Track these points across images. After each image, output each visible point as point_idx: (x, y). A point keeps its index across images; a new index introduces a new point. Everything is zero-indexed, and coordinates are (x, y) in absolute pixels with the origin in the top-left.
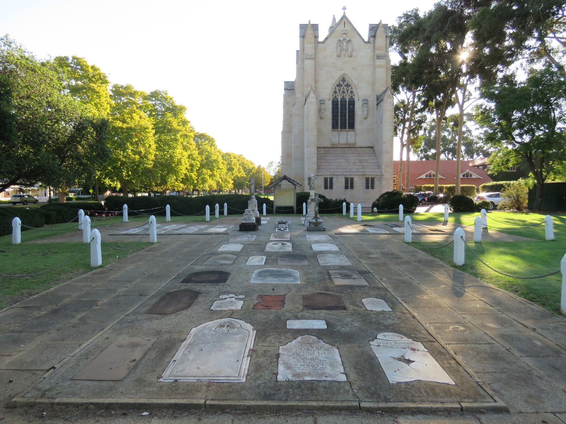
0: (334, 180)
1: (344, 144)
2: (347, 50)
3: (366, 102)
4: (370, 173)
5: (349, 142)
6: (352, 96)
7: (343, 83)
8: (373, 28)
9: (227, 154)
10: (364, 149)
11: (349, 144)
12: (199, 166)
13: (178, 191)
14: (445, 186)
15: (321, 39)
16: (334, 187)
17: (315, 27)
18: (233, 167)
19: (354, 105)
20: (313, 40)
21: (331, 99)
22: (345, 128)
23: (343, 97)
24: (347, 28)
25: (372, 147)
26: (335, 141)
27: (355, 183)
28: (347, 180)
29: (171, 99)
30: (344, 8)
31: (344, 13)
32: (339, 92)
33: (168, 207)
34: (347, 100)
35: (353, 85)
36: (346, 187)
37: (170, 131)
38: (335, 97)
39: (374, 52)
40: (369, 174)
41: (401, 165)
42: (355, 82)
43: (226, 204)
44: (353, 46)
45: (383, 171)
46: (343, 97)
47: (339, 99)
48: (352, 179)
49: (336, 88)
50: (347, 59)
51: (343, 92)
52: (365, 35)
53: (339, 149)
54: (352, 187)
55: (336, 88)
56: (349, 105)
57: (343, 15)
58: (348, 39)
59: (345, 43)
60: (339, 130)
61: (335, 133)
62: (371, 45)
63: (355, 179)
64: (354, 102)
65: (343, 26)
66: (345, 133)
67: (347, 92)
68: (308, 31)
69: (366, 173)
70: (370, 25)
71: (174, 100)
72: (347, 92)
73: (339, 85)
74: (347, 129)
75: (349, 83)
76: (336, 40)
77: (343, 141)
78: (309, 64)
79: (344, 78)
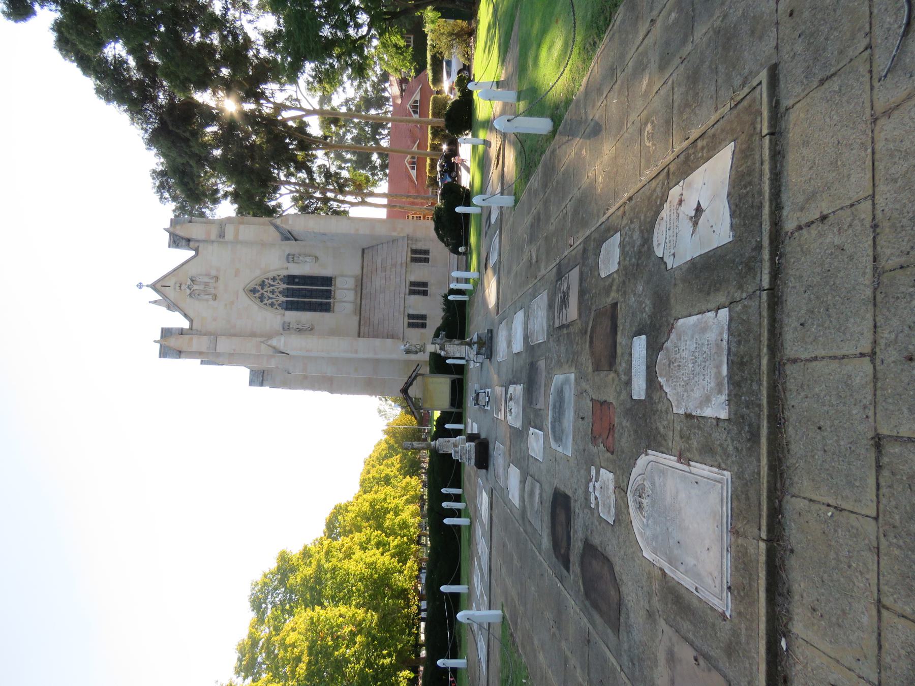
0: (412, 312)
1: (356, 295)
4: (404, 255)
5: (353, 287)
6: (281, 280)
8: (174, 242)
9: (361, 485)
12: (380, 532)
15: (186, 324)
16: (423, 312)
17: (166, 333)
18: (383, 475)
21: (283, 311)
22: (330, 291)
23: (280, 292)
24: (171, 282)
25: (363, 250)
26: (349, 307)
28: (412, 292)
29: (265, 576)
30: (140, 286)
31: (147, 286)
34: (285, 286)
35: (263, 277)
36: (425, 293)
38: (279, 305)
39: (213, 242)
41: (394, 206)
42: (258, 273)
44: (201, 275)
45: (402, 235)
46: (280, 292)
47: (282, 299)
48: (412, 284)
51: (273, 292)
52: (185, 254)
53: (363, 302)
54: (425, 284)
58: (189, 282)
59: (195, 287)
61: (337, 307)
62: (201, 245)
63: (413, 279)
65: (169, 290)
68: (171, 345)
69: (404, 261)
73: (261, 299)
75: (259, 281)
77: (350, 296)
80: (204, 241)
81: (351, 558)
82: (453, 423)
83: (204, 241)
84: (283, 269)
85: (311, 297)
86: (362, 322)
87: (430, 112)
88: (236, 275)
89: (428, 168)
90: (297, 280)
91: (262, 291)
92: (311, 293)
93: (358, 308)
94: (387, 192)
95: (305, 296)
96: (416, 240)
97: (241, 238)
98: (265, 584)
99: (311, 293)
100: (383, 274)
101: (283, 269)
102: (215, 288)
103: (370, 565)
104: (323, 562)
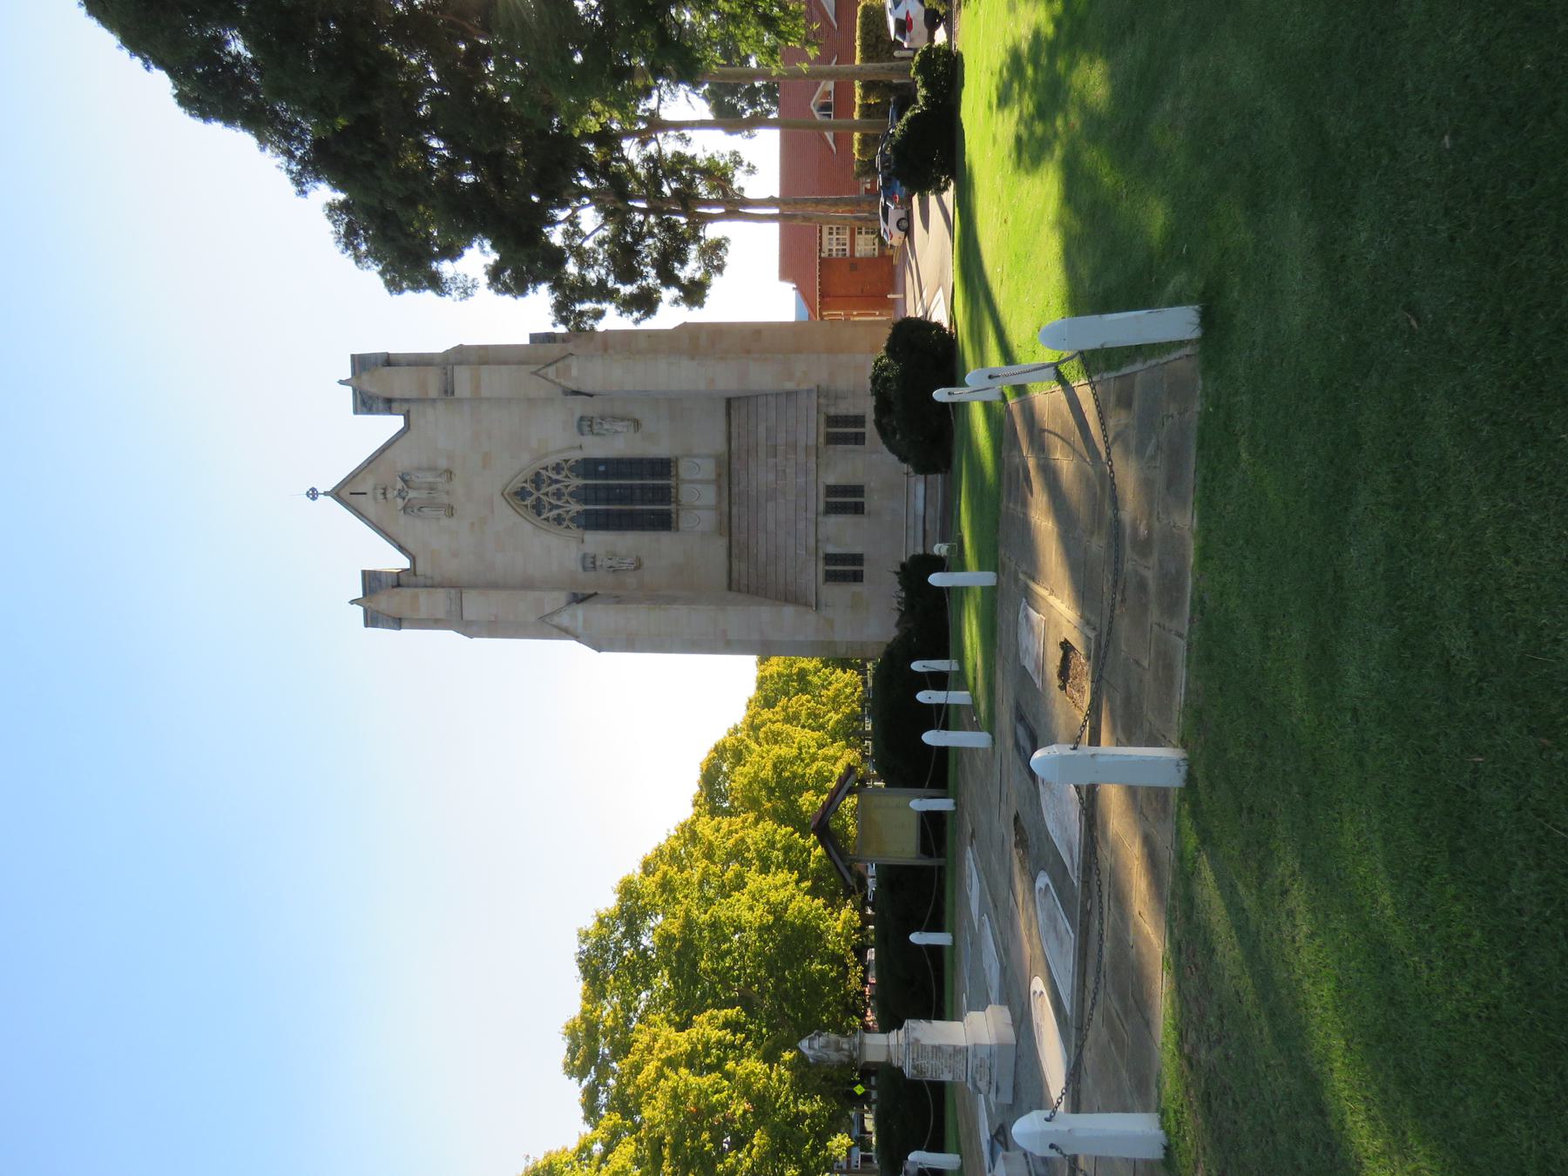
0: (832, 550)
2: (432, 488)
3: (586, 424)
4: (810, 431)
5: (713, 476)
6: (571, 469)
7: (532, 495)
8: (364, 403)
9: (759, 688)
10: (734, 431)
11: (719, 475)
12: (790, 829)
13: (866, 920)
14: (858, 100)
15: (404, 563)
16: (857, 550)
17: (373, 582)
18: (795, 670)
19: (597, 462)
20: (406, 593)
21: (576, 532)
22: (669, 487)
23: (571, 495)
24: (367, 485)
25: (729, 401)
27: (843, 482)
28: (832, 509)
29: (601, 921)
30: (313, 494)
31: (326, 494)
32: (558, 507)
33: (915, 938)
35: (537, 466)
36: (858, 509)
37: (688, 944)
38: (572, 519)
39: (434, 400)
41: (794, 217)
43: (917, 666)
44: (420, 469)
45: (804, 386)
46: (571, 495)
47: (576, 507)
48: (832, 490)
49: (547, 519)
52: (389, 425)
53: (734, 511)
54: (857, 490)
55: (547, 519)
56: (597, 475)
58: (400, 484)
59: (412, 494)
60: (673, 507)
61: (684, 523)
62: (414, 408)
63: (832, 480)
64: (586, 461)
67: (557, 482)
68: (384, 601)
69: (812, 442)
70: (356, 412)
71: (603, 912)
72: (557, 482)
73: (538, 508)
74: (672, 482)
75: (529, 474)
76: (403, 519)
77: (708, 495)
78: (475, 605)
79: (516, 494)
80: (420, 400)
82: (929, 930)
83: (420, 400)
84: (572, 448)
86: (735, 551)
87: (858, 43)
89: (856, 146)
90: (602, 468)
91: (536, 494)
93: (726, 520)
94: (777, 195)
95: (621, 500)
97: (485, 393)
98: (601, 938)
99: (627, 495)
100: (771, 461)
102: (448, 493)
103: (777, 910)
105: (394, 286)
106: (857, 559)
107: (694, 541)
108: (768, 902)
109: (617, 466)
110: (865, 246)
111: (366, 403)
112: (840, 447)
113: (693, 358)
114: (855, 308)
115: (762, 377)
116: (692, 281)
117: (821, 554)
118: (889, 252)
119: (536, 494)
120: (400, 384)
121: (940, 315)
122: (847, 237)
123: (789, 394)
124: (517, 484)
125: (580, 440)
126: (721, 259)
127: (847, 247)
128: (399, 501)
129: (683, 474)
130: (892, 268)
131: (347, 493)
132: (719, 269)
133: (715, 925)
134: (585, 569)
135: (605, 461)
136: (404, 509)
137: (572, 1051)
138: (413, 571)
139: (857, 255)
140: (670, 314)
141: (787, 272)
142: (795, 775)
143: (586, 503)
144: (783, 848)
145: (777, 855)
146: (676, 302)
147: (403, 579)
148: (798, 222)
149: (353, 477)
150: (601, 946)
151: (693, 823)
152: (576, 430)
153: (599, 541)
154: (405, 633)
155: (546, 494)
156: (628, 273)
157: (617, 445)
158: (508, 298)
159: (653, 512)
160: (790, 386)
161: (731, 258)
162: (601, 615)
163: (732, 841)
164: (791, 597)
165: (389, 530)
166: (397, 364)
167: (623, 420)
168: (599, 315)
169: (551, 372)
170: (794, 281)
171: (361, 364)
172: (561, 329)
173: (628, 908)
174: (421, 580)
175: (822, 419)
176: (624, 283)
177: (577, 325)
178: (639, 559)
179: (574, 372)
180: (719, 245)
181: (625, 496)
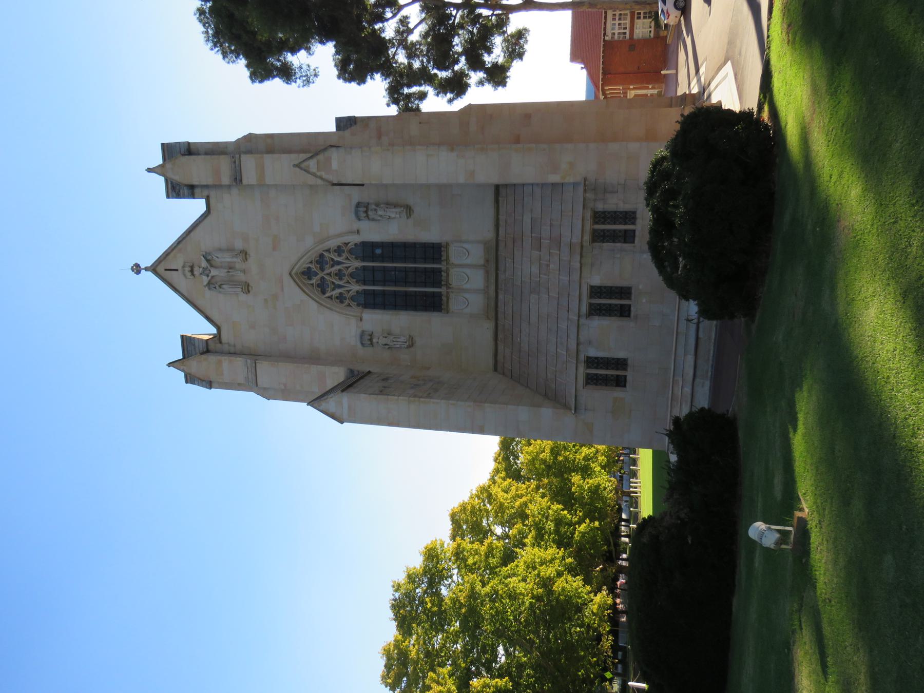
0: (593, 353)
1: (487, 279)
2: (231, 267)
3: (363, 210)
4: (575, 227)
5: (482, 262)
7: (316, 275)
8: (173, 188)
10: (502, 218)
11: (487, 261)
12: (560, 506)
16: (621, 355)
19: (374, 245)
20: (212, 358)
21: (356, 310)
24: (177, 263)
26: (476, 302)
27: (609, 283)
28: (596, 311)
31: (146, 269)
32: (340, 287)
34: (358, 264)
35: (320, 248)
36: (624, 312)
38: (352, 298)
40: (578, 232)
42: (309, 242)
44: (220, 250)
45: (570, 179)
46: (352, 275)
47: (356, 288)
48: (596, 291)
49: (330, 297)
50: (252, 264)
51: (340, 275)
52: (195, 207)
53: (501, 297)
56: (373, 258)
57: (150, 273)
58: (204, 264)
59: (214, 272)
60: (443, 290)
61: (455, 304)
62: (213, 194)
63: (597, 281)
64: (364, 244)
65: (178, 268)
66: (453, 272)
67: (339, 263)
68: (199, 361)
69: (576, 240)
70: (168, 197)
72: (339, 263)
73: (322, 287)
74: (443, 266)
75: (313, 255)
77: (477, 280)
78: (265, 370)
79: (303, 273)
80: (218, 187)
81: (524, 545)
84: (351, 232)
85: (406, 283)
86: (500, 336)
88: (274, 249)
90: (378, 251)
91: (321, 275)
92: (405, 277)
95: (396, 282)
96: (605, 191)
97: (269, 181)
99: (405, 277)
100: (536, 253)
101: (351, 232)
102: (244, 271)
104: (478, 587)
105: (339, 77)
106: (621, 364)
107: (456, 330)
108: (538, 575)
109: (393, 250)
110: (643, 29)
111: (175, 190)
112: (607, 245)
113: (452, 150)
114: (632, 83)
115: (524, 168)
116: (495, 66)
117: (582, 357)
118: (663, 33)
119: (321, 275)
120: (197, 171)
121: (730, 94)
122: (628, 22)
123: (554, 185)
124: (303, 265)
125: (357, 225)
126: (522, 47)
127: (627, 31)
128: (205, 278)
129: (453, 259)
130: (666, 47)
131: (161, 268)
132: (520, 56)
133: (494, 597)
134: (362, 344)
135: (381, 245)
136: (209, 283)
137: (388, 667)
138: (218, 337)
139: (635, 37)
140: (479, 94)
141: (576, 55)
142: (566, 459)
143: (365, 284)
144: (556, 520)
145: (550, 526)
146: (481, 83)
147: (212, 346)
148: (585, 9)
149: (167, 254)
150: (409, 597)
151: (489, 487)
152: (353, 216)
153: (375, 320)
154: (215, 392)
155: (329, 274)
156: (444, 58)
157: (390, 230)
158: (354, 85)
159: (425, 294)
160: (554, 178)
161: (531, 47)
162: (361, 400)
163: (517, 504)
164: (550, 395)
165: (198, 303)
166: (197, 153)
167: (396, 206)
168: (423, 96)
169: (312, 164)
170: (583, 62)
171: (169, 150)
172: (393, 110)
173: (430, 569)
174: (226, 348)
175: (589, 214)
176: (439, 69)
177: (407, 105)
178: (411, 338)
179: (335, 165)
180: (520, 35)
181: (400, 276)
